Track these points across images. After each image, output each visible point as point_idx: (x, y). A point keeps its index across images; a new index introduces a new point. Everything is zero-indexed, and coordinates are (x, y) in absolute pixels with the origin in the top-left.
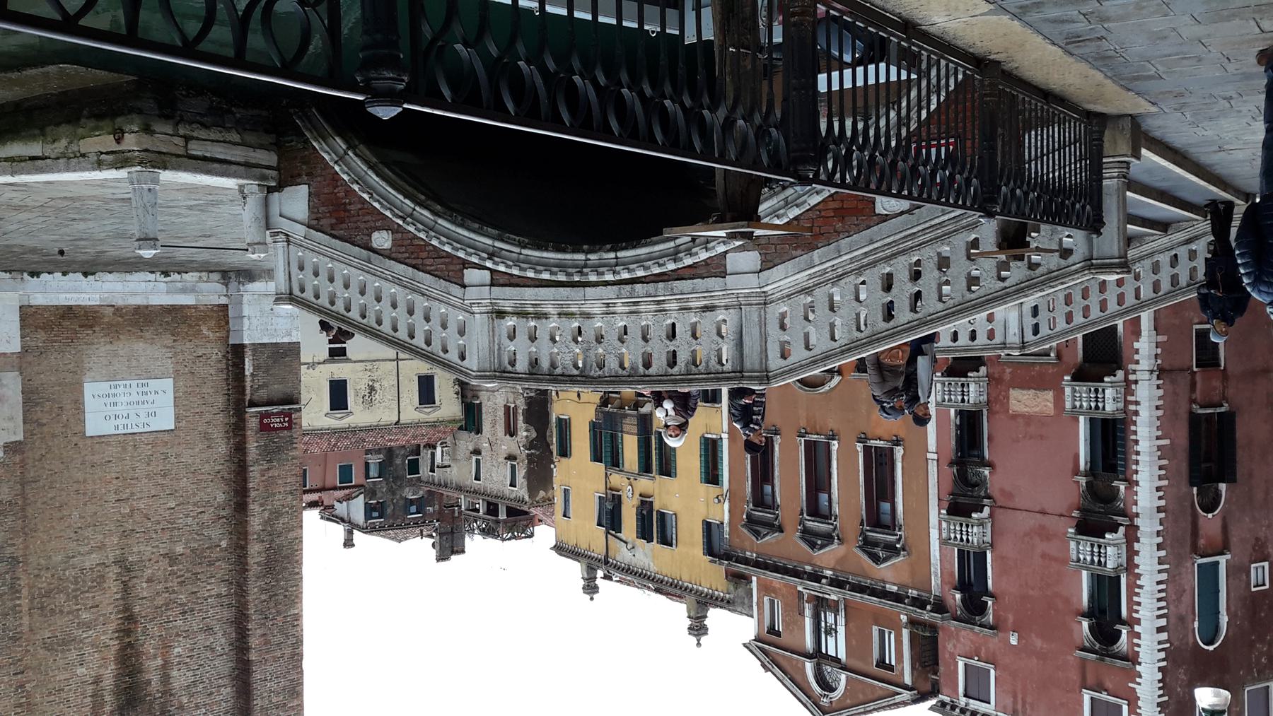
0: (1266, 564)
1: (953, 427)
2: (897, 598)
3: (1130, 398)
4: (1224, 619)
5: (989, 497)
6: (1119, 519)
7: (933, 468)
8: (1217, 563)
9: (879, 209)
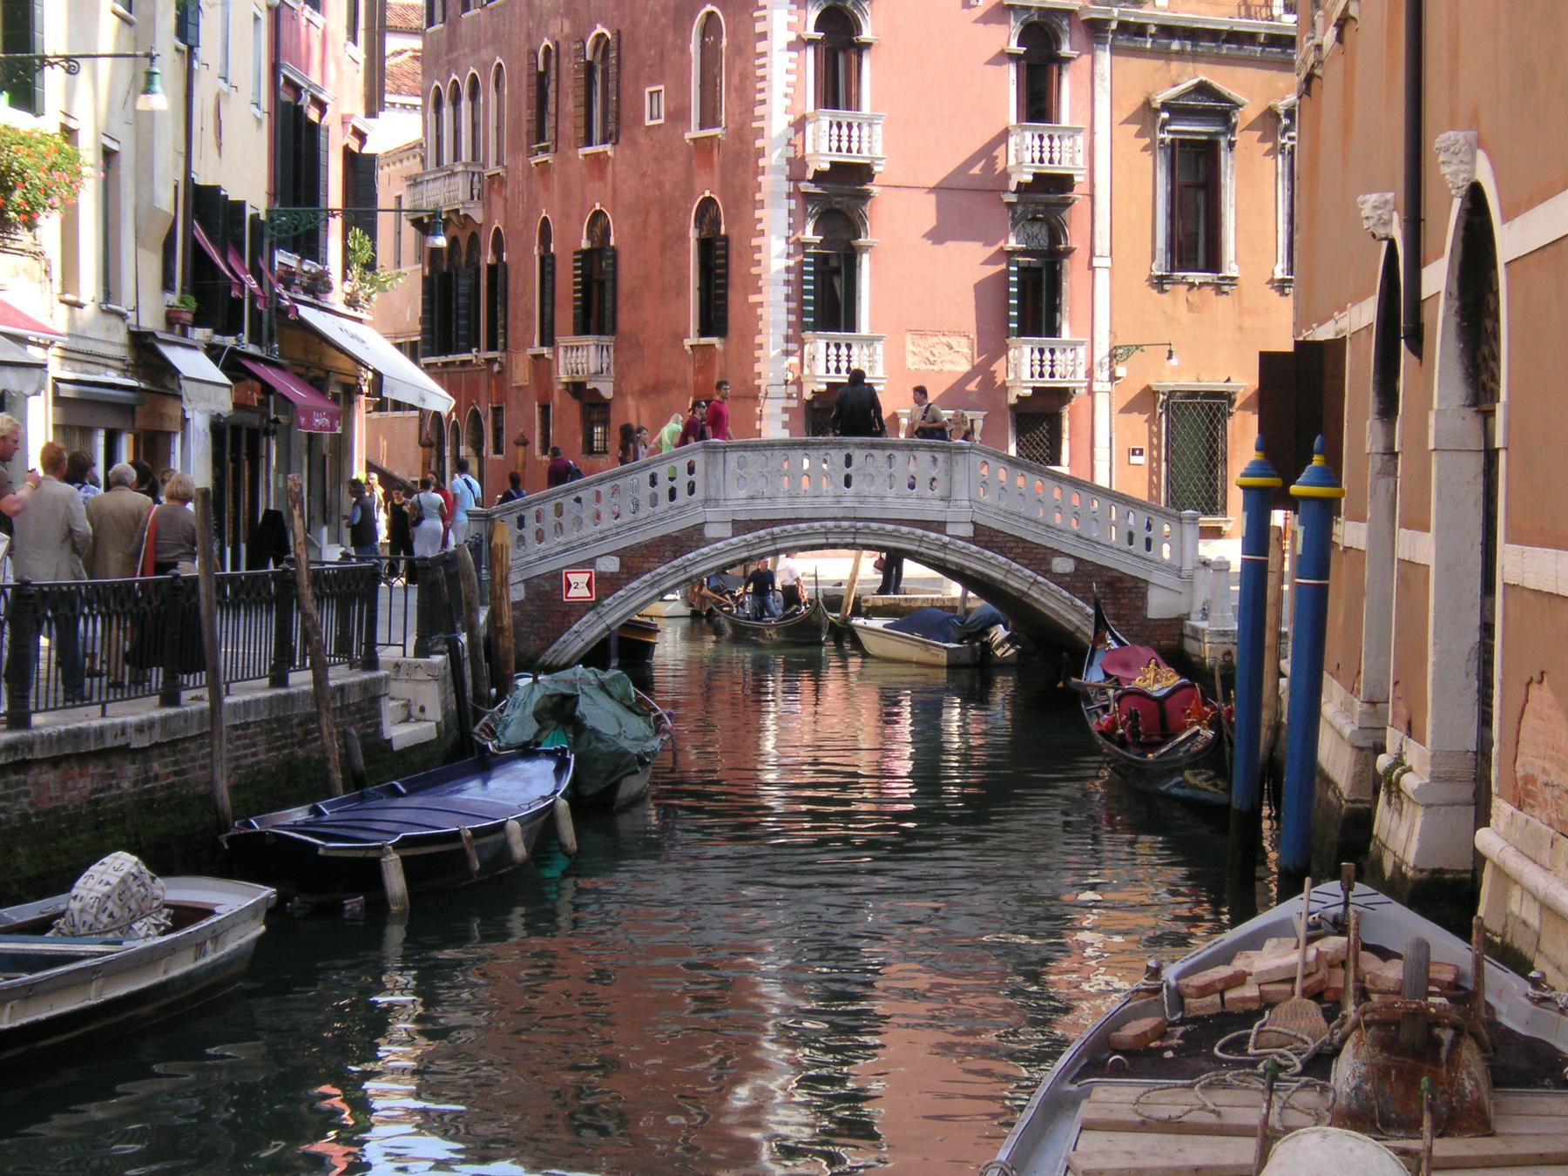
0: (648, 122)
4: (694, 48)
5: (1009, 205)
6: (812, 188)
8: (702, 126)
9: (616, 560)
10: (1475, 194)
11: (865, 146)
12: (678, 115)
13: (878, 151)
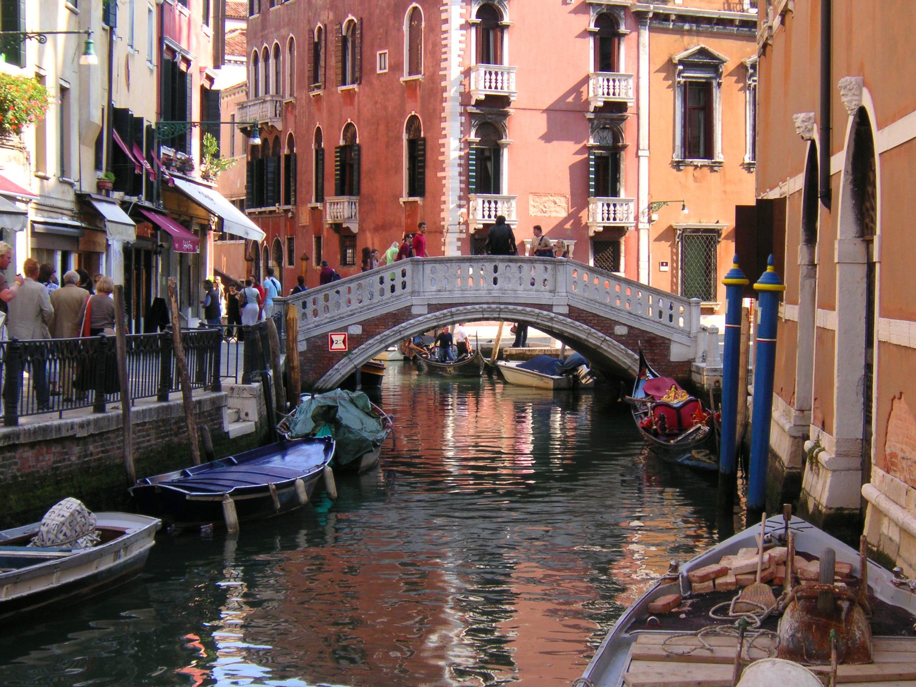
0: (379, 72)
4: (405, 28)
5: (590, 120)
6: (474, 110)
8: (410, 74)
9: (360, 327)
10: (862, 113)
11: (505, 85)
12: (396, 67)
13: (513, 88)
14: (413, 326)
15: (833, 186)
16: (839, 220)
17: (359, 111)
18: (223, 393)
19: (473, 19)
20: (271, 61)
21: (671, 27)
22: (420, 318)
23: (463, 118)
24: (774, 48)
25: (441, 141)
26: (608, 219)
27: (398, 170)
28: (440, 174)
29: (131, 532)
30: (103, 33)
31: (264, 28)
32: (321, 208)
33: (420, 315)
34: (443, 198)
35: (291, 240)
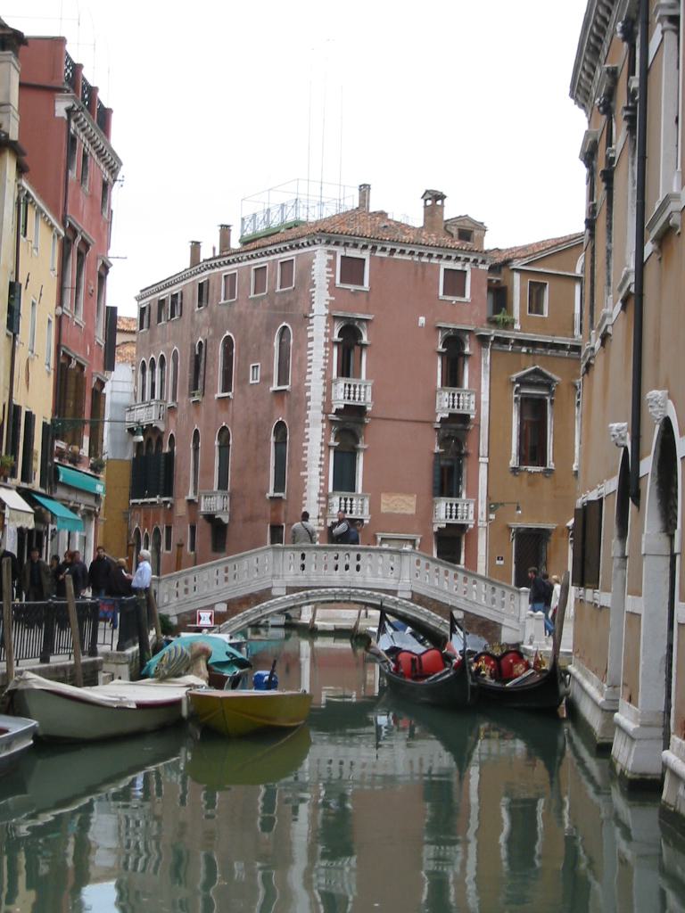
0: (251, 382)
1: (464, 482)
2: (520, 342)
3: (324, 506)
4: (276, 343)
5: (436, 429)
7: (483, 449)
9: (226, 605)
10: (667, 423)
12: (267, 379)
14: (272, 605)
15: (642, 486)
16: (648, 516)
17: (233, 418)
18: (99, 658)
19: (336, 337)
20: (157, 370)
21: (510, 349)
22: (279, 599)
23: (325, 425)
24: (595, 367)
25: (304, 444)
26: (451, 517)
27: (267, 468)
28: (302, 474)
29: (13, 731)
30: (7, 339)
31: (151, 341)
32: (197, 501)
33: (279, 596)
34: (304, 495)
35: (169, 529)
